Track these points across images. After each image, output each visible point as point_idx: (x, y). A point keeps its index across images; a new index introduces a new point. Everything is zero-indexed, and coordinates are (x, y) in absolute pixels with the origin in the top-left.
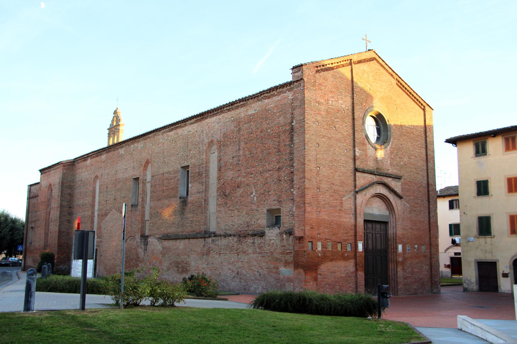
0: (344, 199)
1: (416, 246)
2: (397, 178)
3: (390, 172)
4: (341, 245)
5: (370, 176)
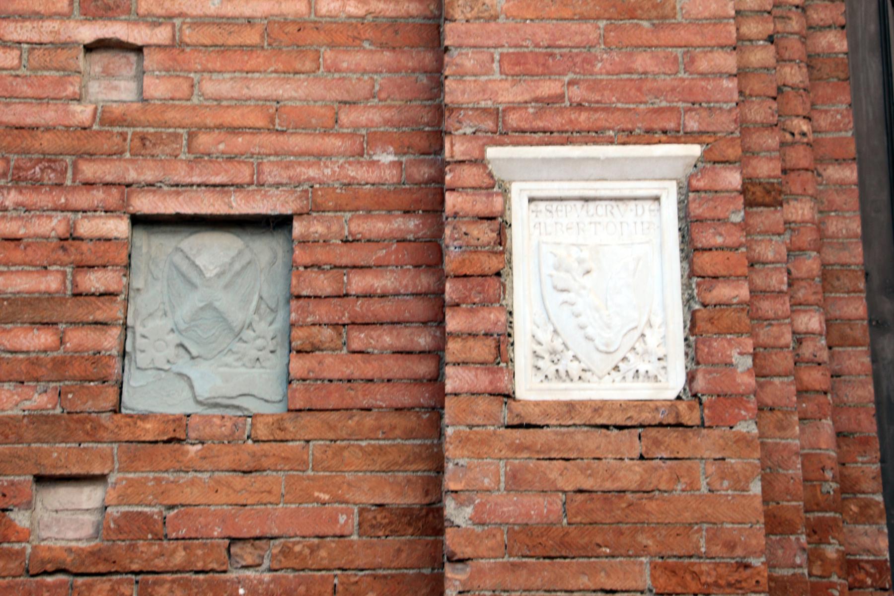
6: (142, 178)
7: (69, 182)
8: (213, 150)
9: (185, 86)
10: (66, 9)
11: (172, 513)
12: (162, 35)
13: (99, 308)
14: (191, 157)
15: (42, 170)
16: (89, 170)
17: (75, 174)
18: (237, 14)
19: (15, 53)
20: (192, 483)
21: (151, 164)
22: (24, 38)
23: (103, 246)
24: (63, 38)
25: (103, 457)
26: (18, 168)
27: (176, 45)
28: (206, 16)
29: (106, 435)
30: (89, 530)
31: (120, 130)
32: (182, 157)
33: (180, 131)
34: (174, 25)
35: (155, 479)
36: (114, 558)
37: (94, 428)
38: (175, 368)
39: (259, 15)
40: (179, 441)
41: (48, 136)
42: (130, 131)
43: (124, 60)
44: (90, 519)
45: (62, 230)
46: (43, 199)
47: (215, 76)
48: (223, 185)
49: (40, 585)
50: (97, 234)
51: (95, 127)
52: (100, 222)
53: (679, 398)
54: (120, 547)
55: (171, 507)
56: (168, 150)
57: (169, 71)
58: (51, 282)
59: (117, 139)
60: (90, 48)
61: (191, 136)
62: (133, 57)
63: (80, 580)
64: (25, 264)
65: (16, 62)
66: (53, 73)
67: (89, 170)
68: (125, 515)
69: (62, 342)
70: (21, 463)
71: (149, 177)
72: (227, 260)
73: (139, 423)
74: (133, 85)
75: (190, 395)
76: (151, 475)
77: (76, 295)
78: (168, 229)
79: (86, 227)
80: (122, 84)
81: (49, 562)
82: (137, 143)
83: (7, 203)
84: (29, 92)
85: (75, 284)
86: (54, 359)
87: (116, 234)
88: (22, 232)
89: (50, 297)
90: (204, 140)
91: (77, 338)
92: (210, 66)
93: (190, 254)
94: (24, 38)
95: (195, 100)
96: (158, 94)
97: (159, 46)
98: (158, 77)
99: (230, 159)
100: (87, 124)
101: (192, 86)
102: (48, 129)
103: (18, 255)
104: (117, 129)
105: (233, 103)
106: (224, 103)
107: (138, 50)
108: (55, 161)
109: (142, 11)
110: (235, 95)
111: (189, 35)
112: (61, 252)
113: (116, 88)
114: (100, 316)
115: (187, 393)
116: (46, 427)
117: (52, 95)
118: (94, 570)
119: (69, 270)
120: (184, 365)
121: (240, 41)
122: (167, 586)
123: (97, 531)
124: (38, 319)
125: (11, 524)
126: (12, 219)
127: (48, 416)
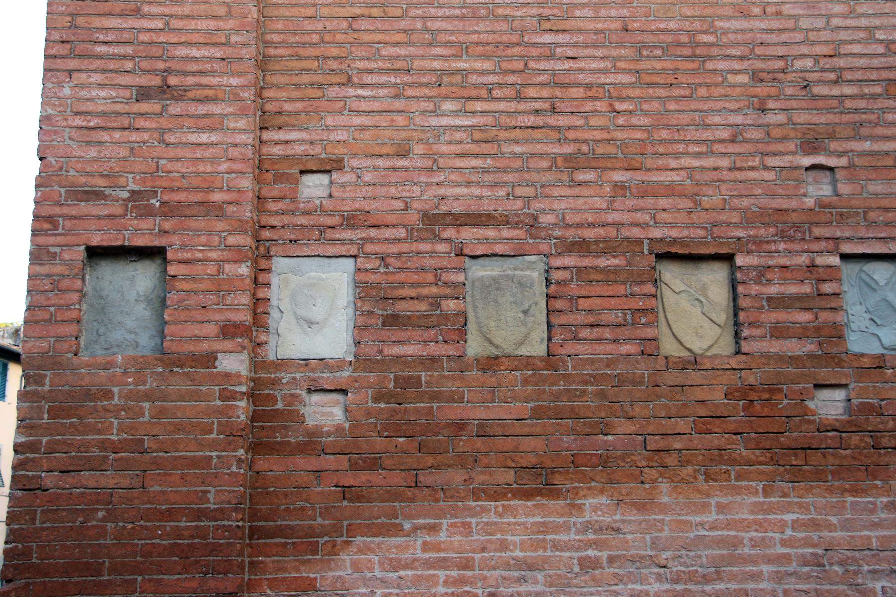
4: (734, 284)
6: (843, 235)
7: (808, 238)
8: (877, 220)
9: (859, 187)
10: (794, 149)
11: (883, 403)
12: (843, 161)
13: (832, 301)
14: (866, 224)
15: (794, 232)
16: (817, 232)
17: (810, 233)
18: (880, 149)
19: (773, 172)
20: (891, 388)
21: (847, 228)
22: (776, 165)
23: (829, 270)
24: (795, 164)
25: (846, 375)
26: (782, 231)
27: (851, 166)
28: (865, 151)
29: (846, 365)
30: (841, 411)
31: (829, 210)
32: (862, 224)
33: (859, 210)
34: (849, 156)
35: (873, 386)
36: (859, 424)
37: (839, 361)
38: (870, 331)
39: (891, 150)
40: (880, 367)
41: (795, 214)
42: (834, 211)
43: (823, 174)
44: (841, 405)
45: (808, 262)
46: (797, 247)
47: (873, 182)
48: (884, 238)
49: (827, 437)
50: (826, 264)
51: (817, 210)
52: (826, 258)
53: (358, 343)
54: (861, 419)
55: (882, 400)
56: (854, 221)
57: (850, 180)
58: (807, 289)
59: (829, 215)
60: (807, 169)
61: (865, 213)
62: (828, 173)
63: (844, 435)
64: (793, 279)
65: (774, 177)
66: (792, 182)
67: (817, 232)
68: (861, 403)
69: (817, 318)
70: (807, 378)
71: (847, 234)
72: (889, 276)
73: (861, 359)
74: (829, 187)
75: (879, 345)
76: (870, 384)
77: (819, 295)
78: (855, 260)
79: (820, 260)
80: (824, 187)
81: (829, 426)
82: (838, 217)
83: (780, 249)
84: (783, 192)
85: (818, 289)
86: (814, 327)
87: (835, 264)
88: (789, 263)
89: (807, 296)
90: (872, 215)
91: (824, 316)
92: (870, 177)
93: (870, 273)
94: (776, 165)
95: (864, 195)
96: (845, 192)
97: (843, 167)
98: (844, 183)
99: (886, 225)
100: (813, 208)
101: (862, 187)
102: (794, 211)
103: (789, 275)
104: (827, 210)
105: (884, 195)
106: (879, 196)
107: (831, 169)
108: (800, 227)
109: (832, 149)
110: (884, 192)
111: (857, 161)
112: (808, 273)
113: (821, 189)
114: (833, 305)
115: (878, 344)
116: (816, 360)
117: (794, 194)
118: (850, 430)
119: (814, 282)
120: (873, 329)
121: (883, 164)
122: (887, 438)
123: (845, 411)
124: (804, 307)
125: (807, 407)
126: (783, 257)
127: (816, 355)
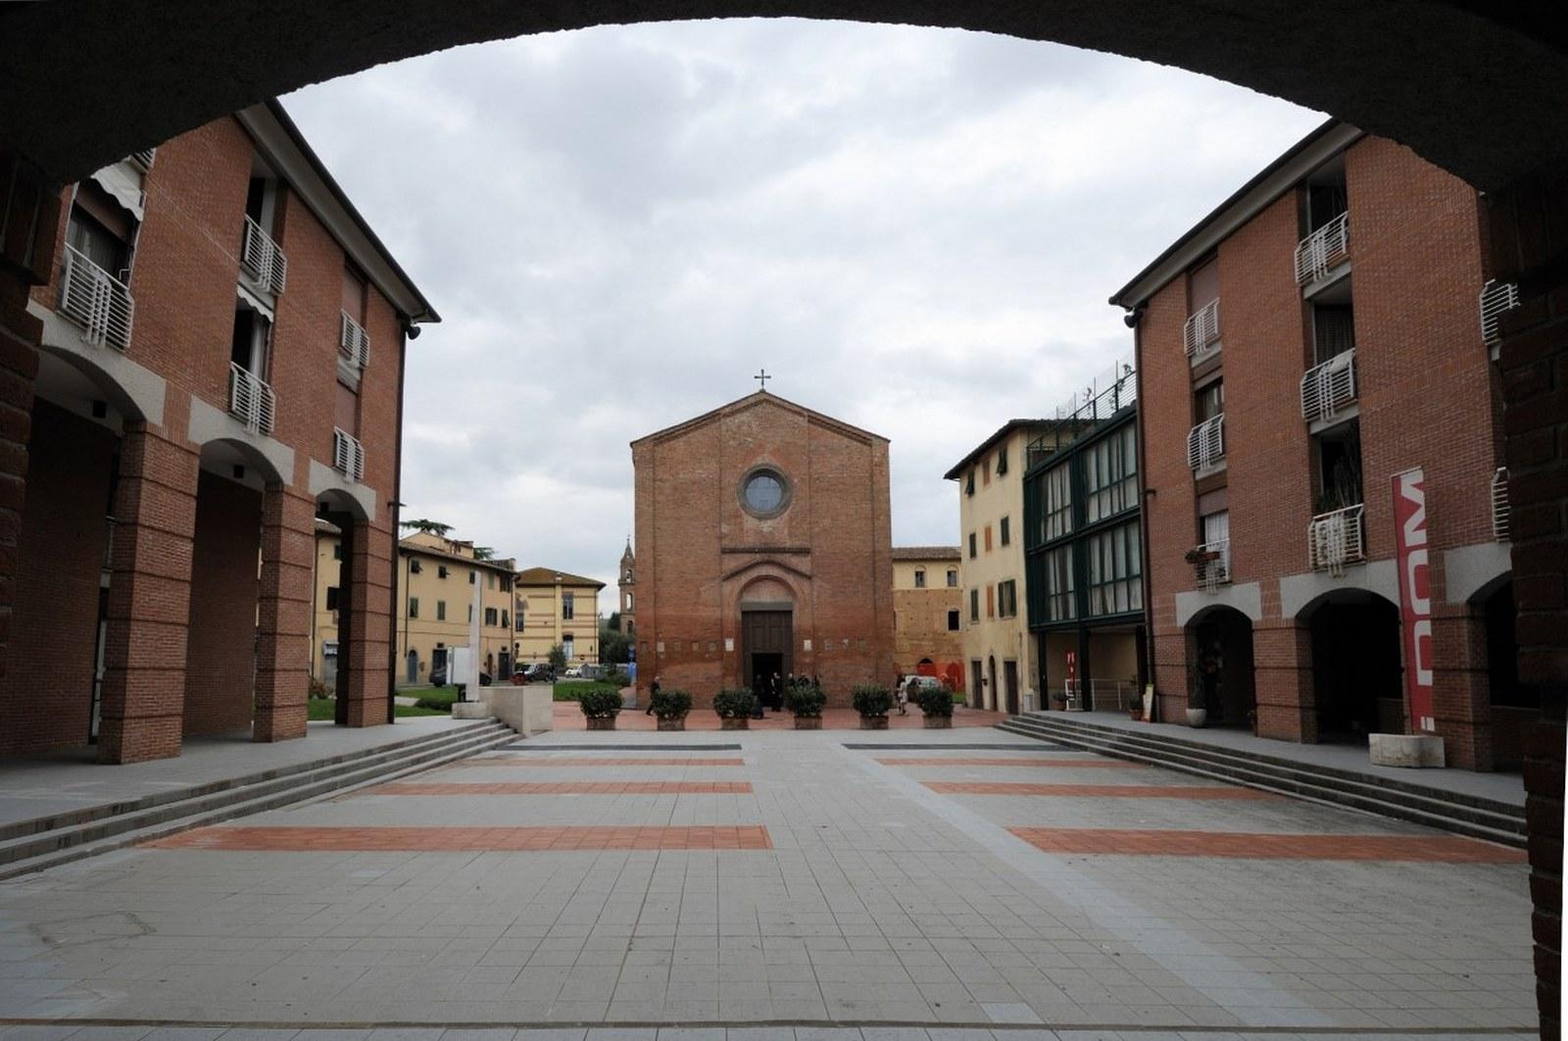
0: (702, 589)
1: (846, 641)
2: (803, 552)
3: (788, 545)
5: (749, 555)
